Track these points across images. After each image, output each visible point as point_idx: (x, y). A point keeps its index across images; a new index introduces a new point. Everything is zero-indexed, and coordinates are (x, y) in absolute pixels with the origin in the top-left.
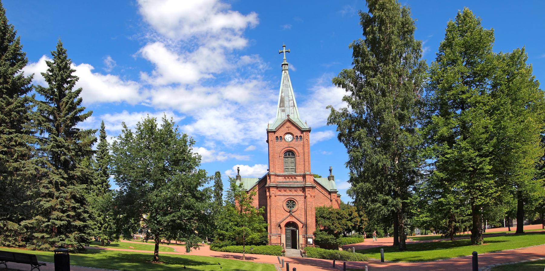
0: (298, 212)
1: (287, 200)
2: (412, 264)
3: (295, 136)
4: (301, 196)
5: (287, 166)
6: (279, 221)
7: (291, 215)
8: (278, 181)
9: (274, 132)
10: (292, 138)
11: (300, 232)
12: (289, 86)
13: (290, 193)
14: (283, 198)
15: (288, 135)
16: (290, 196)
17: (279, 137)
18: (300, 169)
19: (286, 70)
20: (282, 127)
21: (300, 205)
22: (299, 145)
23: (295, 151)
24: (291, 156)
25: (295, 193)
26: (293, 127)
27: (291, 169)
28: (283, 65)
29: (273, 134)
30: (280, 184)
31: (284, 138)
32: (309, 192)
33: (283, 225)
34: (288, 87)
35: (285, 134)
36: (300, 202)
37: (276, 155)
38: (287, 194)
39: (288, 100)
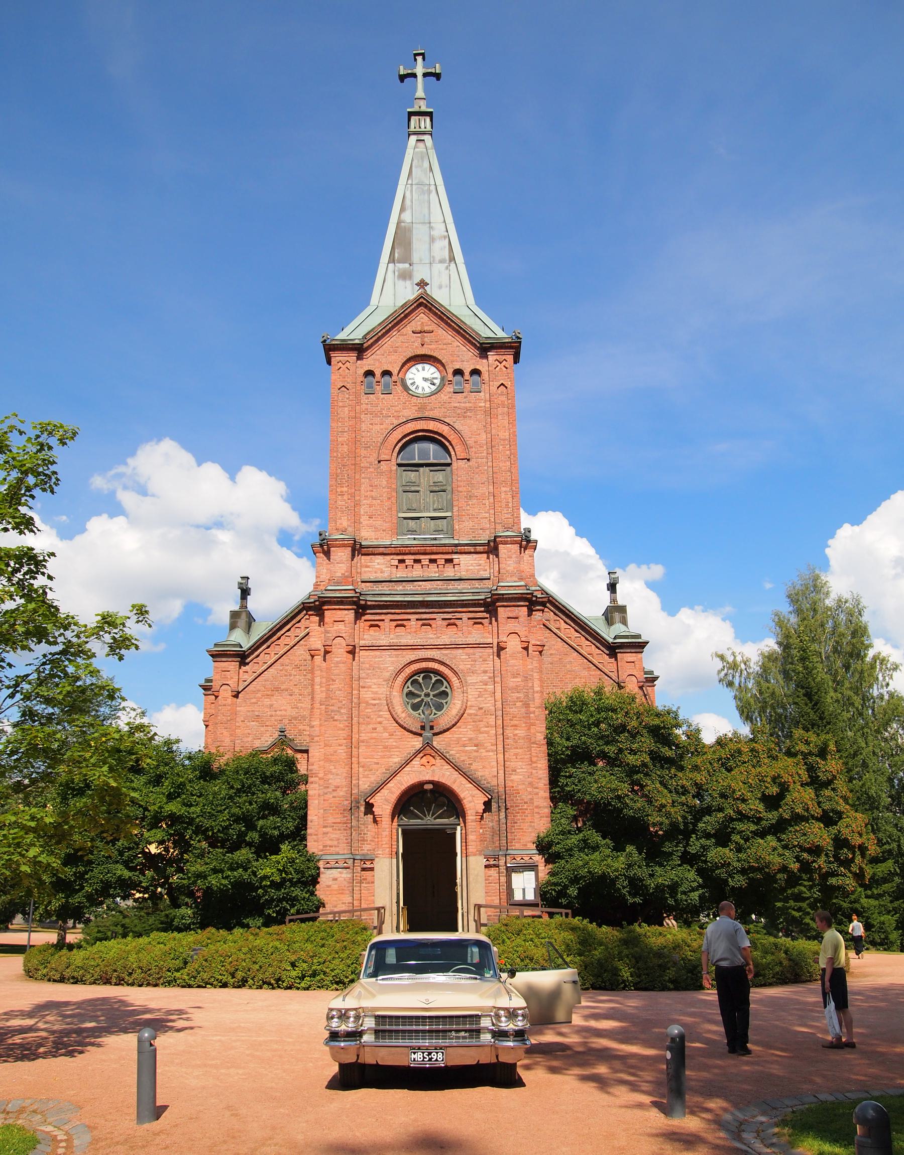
0: (463, 732)
1: (409, 671)
2: (806, 997)
3: (450, 371)
4: (478, 646)
5: (414, 506)
6: (365, 784)
7: (428, 749)
8: (365, 578)
9: (360, 350)
10: (437, 382)
11: (471, 837)
12: (433, 188)
13: (428, 636)
14: (391, 662)
15: (420, 366)
16: (423, 647)
17: (378, 373)
18: (472, 517)
19: (424, 133)
20: (394, 332)
21: (472, 693)
22: (468, 409)
23: (452, 437)
24: (432, 461)
25: (448, 636)
26: (444, 334)
27: (433, 518)
28: (411, 114)
29: (352, 357)
30: (385, 588)
31: (403, 382)
32: (512, 626)
33: (384, 803)
34: (429, 192)
35: (409, 360)
36: (471, 679)
37: (363, 452)
38: (411, 642)
39: (427, 239)
